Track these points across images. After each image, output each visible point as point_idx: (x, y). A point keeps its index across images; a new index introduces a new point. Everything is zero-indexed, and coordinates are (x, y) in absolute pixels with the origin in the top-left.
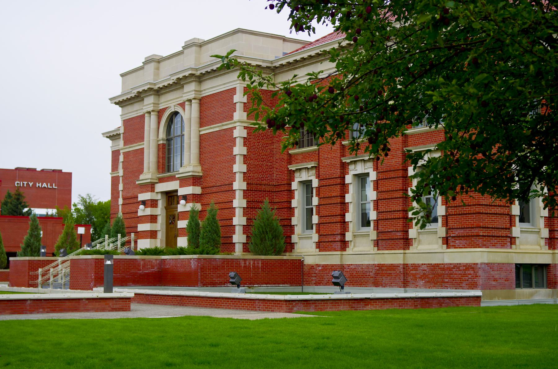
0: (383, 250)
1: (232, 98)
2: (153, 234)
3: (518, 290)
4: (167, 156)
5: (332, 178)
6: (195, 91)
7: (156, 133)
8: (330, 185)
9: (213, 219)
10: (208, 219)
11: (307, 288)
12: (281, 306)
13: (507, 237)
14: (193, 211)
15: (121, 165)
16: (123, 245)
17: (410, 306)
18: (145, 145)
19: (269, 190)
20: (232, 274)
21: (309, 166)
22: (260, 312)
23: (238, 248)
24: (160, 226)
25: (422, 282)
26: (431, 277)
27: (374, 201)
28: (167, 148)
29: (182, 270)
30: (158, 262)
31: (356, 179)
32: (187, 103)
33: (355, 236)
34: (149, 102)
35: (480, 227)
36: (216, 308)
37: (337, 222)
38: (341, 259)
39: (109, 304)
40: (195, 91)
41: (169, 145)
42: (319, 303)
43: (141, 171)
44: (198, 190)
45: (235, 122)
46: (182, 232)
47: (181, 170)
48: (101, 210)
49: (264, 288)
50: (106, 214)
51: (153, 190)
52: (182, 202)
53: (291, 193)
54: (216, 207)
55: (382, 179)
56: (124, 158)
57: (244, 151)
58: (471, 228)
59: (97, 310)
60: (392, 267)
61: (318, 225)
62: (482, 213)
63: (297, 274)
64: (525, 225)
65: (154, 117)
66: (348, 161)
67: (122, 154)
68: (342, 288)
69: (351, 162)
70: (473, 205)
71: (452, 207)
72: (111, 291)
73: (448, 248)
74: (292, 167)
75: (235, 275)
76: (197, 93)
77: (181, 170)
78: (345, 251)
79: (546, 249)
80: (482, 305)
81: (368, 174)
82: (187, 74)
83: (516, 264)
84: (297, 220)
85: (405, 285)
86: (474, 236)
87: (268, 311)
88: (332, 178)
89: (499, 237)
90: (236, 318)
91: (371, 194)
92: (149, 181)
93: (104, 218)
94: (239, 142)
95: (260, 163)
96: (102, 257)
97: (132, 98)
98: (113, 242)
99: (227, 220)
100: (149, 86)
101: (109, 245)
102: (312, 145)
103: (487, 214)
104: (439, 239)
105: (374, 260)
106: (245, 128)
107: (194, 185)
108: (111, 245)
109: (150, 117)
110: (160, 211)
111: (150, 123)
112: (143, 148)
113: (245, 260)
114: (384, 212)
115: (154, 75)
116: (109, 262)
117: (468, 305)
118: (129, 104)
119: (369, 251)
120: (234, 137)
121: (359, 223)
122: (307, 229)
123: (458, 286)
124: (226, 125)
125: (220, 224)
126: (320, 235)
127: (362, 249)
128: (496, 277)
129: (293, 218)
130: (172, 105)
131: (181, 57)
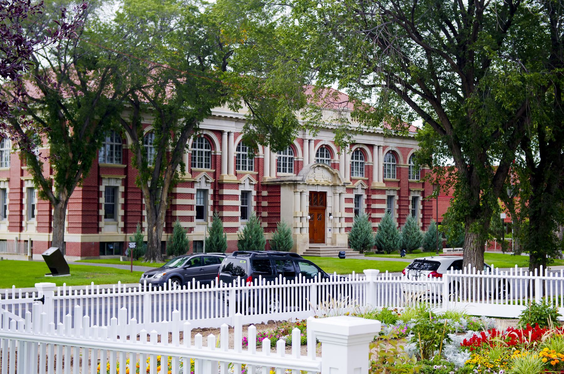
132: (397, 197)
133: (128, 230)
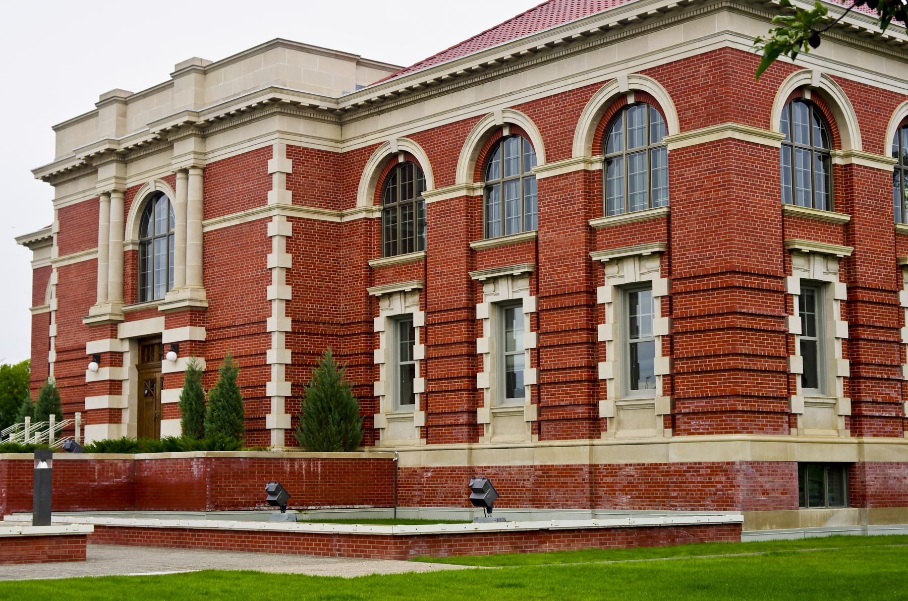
0: (549, 439)
1: (265, 165)
2: (113, 416)
3: (803, 511)
4: (140, 273)
5: (451, 310)
6: (195, 153)
7: (121, 231)
8: (448, 323)
9: (230, 385)
10: (221, 386)
11: (404, 512)
12: (386, 548)
13: (783, 413)
14: (192, 372)
15: (51, 290)
16: (58, 434)
17: (620, 543)
18: (99, 253)
19: (332, 336)
20: (272, 486)
21: (408, 289)
22: (342, 559)
23: (277, 441)
24: (127, 399)
25: (625, 499)
26: (643, 487)
27: (532, 349)
28: (140, 258)
29: (174, 479)
30: (128, 465)
31: (497, 312)
32: (179, 175)
33: (494, 415)
34: (108, 175)
35: (738, 396)
36: (251, 551)
37: (461, 390)
38: (470, 457)
39: (43, 548)
40: (195, 153)
41: (145, 253)
42: (456, 541)
43: (92, 301)
44: (200, 334)
45: (271, 209)
46: (171, 410)
47: (169, 297)
48: (8, 378)
49: (326, 511)
50: (16, 387)
51: (114, 335)
52: (171, 355)
53: (372, 338)
54: (236, 363)
55: (547, 310)
56: (60, 277)
57: (287, 261)
58: (721, 397)
59: (19, 561)
60: (569, 471)
61: (425, 395)
62: (741, 370)
63: (386, 485)
64: (811, 392)
65: (116, 202)
66: (482, 278)
67: (55, 271)
68: (490, 510)
69: (488, 279)
70: (724, 355)
71: (683, 359)
72: (47, 522)
73: (674, 434)
74: (375, 291)
75: (277, 487)
76: (197, 156)
77: (169, 297)
78: (477, 441)
79: (846, 436)
80: (745, 539)
81: (519, 302)
82: (180, 122)
83: (800, 463)
84: (385, 387)
85: (594, 502)
86: (726, 412)
87: (358, 556)
88: (451, 310)
89: (769, 413)
90: (312, 574)
91: (526, 338)
92: (107, 318)
93: (11, 393)
94: (278, 245)
95: (316, 284)
96: (30, 456)
97: (75, 169)
98: (40, 430)
99: (255, 387)
100: (107, 146)
101: (32, 435)
102: (411, 251)
103: (749, 370)
104: (658, 418)
105: (533, 458)
106: (289, 219)
107: (192, 324)
108: (38, 435)
109: (110, 202)
110: (127, 372)
111: (110, 214)
112: (97, 259)
113: (292, 460)
114: (551, 370)
115: (117, 127)
116: (43, 465)
117: (720, 539)
118: (70, 180)
119: (523, 442)
120: (269, 235)
121: (502, 391)
122: (402, 403)
123: (696, 504)
124: (254, 215)
125: (243, 394)
126: (428, 415)
127: (509, 439)
128: (767, 486)
129: (376, 383)
130: (151, 180)
131: (168, 93)
132: (840, 291)
133: (866, 424)
